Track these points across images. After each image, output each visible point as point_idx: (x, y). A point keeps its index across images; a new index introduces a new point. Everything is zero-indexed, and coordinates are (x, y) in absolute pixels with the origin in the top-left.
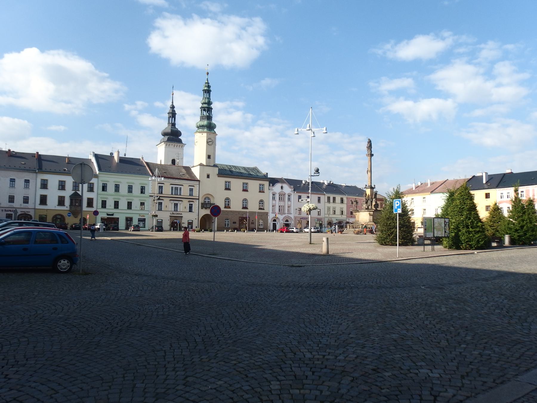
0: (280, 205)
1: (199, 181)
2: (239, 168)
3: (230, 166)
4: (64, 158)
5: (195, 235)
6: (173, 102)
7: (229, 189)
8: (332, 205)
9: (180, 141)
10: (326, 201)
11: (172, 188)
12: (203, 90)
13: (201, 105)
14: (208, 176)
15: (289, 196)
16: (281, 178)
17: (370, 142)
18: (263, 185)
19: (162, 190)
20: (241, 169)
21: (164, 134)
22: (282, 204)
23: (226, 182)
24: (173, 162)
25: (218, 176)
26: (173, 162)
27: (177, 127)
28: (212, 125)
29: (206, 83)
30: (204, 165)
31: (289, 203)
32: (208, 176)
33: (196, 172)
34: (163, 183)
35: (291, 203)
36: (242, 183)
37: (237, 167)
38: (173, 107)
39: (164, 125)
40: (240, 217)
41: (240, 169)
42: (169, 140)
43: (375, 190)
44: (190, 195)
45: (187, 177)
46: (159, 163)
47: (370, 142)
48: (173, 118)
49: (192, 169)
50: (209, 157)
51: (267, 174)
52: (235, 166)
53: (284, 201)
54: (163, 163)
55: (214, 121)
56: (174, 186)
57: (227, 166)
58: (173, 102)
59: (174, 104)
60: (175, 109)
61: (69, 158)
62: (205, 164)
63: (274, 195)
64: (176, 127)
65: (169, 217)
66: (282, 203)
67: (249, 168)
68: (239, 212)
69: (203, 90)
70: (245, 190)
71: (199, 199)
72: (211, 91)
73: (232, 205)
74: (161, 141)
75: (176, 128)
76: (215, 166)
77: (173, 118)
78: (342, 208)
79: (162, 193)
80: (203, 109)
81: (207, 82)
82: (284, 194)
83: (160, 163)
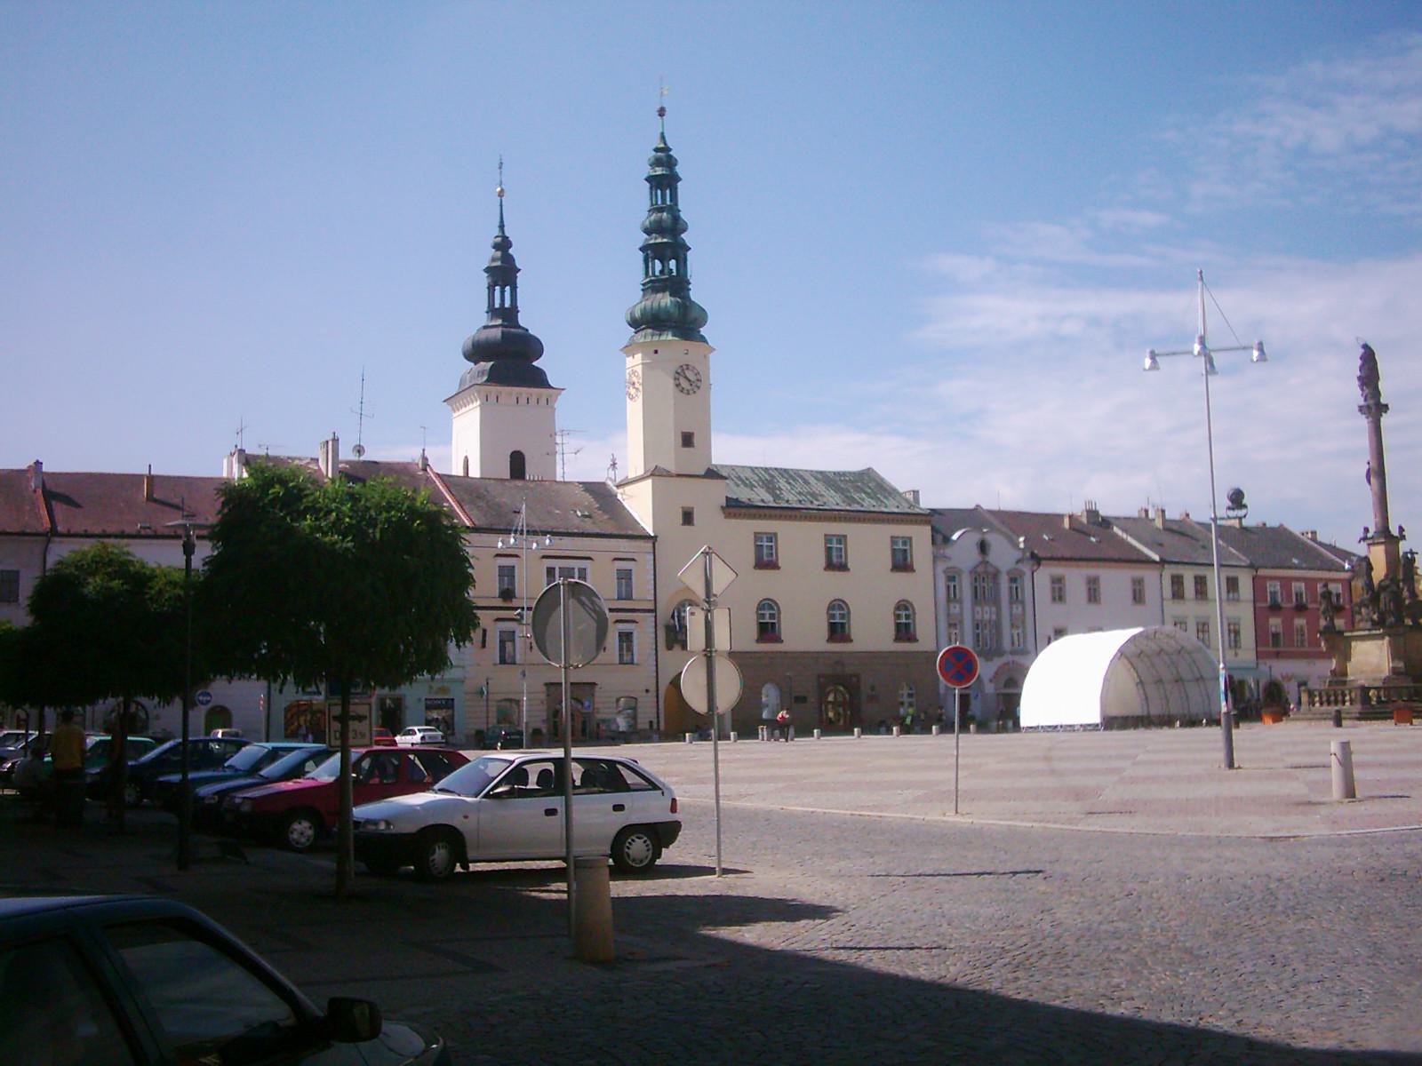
0: (978, 617)
1: (653, 539)
2: (801, 477)
3: (766, 470)
4: (133, 480)
5: (207, 790)
6: (502, 227)
7: (843, 567)
8: (1190, 609)
9: (539, 380)
10: (1168, 592)
11: (550, 571)
12: (649, 179)
13: (642, 238)
14: (688, 517)
15: (1013, 580)
16: (971, 506)
17: (1369, 359)
18: (908, 541)
19: (629, 585)
20: (812, 481)
21: (477, 352)
22: (987, 613)
23: (757, 536)
24: (518, 463)
25: (728, 516)
26: (518, 463)
27: (523, 320)
28: (694, 314)
29: (657, 150)
30: (668, 474)
31: (1017, 610)
32: (688, 517)
33: (640, 505)
34: (633, 560)
35: (962, 609)
36: (888, 541)
37: (797, 472)
38: (503, 245)
39: (474, 320)
40: (819, 676)
41: (806, 482)
42: (495, 378)
43: (1403, 547)
44: (620, 598)
45: (603, 523)
46: (458, 471)
47: (1369, 359)
48: (508, 288)
49: (621, 494)
50: (687, 440)
51: (916, 493)
52: (785, 470)
53: (996, 601)
54: (475, 472)
55: (696, 295)
56: (557, 564)
57: (752, 469)
58: (502, 227)
59: (507, 234)
60: (511, 251)
61: (151, 479)
62: (672, 468)
63: (951, 578)
64: (521, 323)
65: (544, 688)
66: (986, 608)
67: (844, 474)
68: (816, 656)
69: (649, 179)
70: (766, 561)
71: (654, 611)
72: (678, 179)
73: (786, 627)
74: (462, 382)
75: (520, 327)
76: (712, 474)
77: (508, 288)
78: (903, 606)
79: (629, 597)
80: (651, 252)
81: (662, 145)
82: (995, 575)
83: (461, 473)
